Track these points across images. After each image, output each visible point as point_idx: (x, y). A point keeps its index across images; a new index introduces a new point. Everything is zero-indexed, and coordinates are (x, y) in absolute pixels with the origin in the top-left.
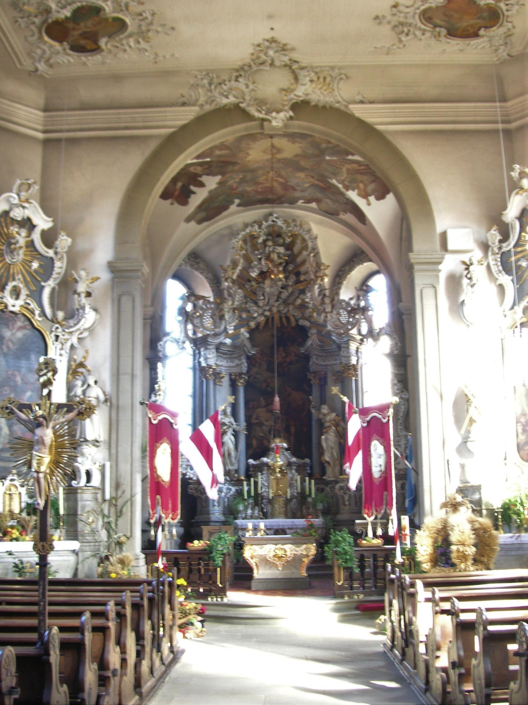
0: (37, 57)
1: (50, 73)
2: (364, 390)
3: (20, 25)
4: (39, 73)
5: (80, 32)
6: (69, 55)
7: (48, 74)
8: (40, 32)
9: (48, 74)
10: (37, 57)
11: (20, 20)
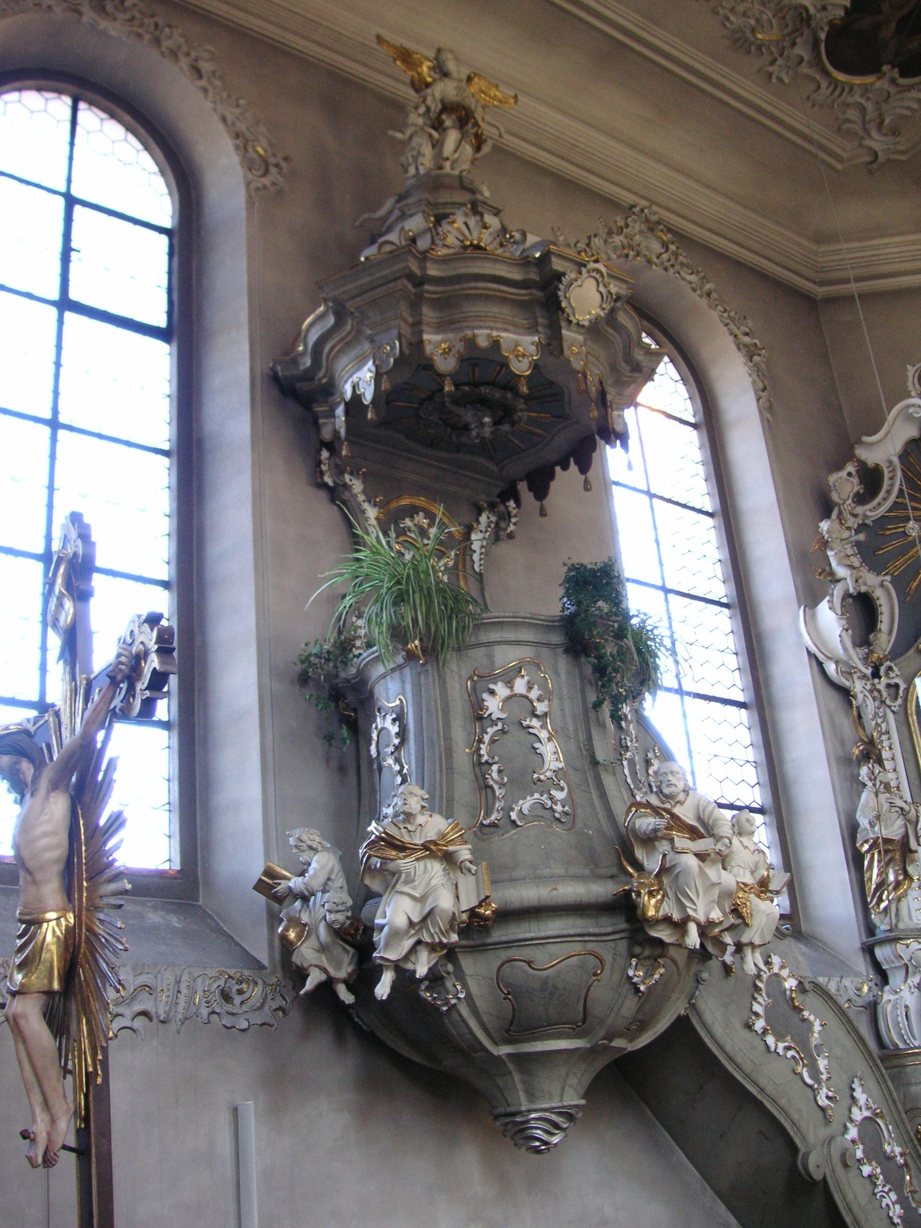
0: (857, 128)
1: (900, 148)
2: (748, 1067)
3: (780, 80)
4: (881, 159)
5: (892, 27)
6: (910, 88)
7: (901, 152)
8: (827, 74)
9: (901, 152)
10: (857, 128)
11: (773, 69)
